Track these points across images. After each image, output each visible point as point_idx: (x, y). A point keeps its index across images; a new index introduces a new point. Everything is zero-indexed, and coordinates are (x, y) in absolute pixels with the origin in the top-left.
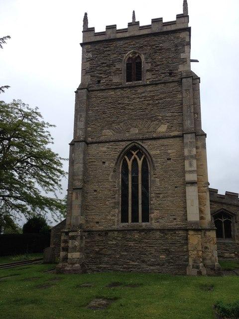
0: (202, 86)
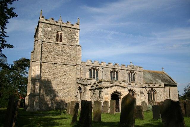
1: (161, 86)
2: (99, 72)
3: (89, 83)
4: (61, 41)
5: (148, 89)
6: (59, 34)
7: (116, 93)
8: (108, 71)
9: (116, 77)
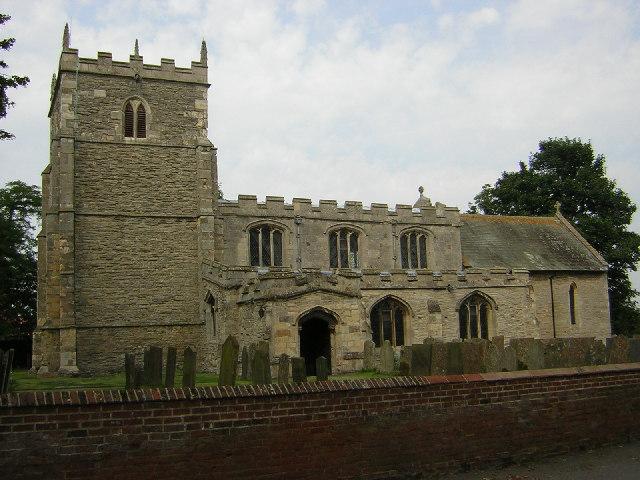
0: (218, 154)
1: (517, 283)
2: (285, 237)
3: (234, 282)
4: (142, 133)
5: (461, 294)
6: (135, 110)
7: (316, 315)
8: (318, 231)
9: (275, 258)
